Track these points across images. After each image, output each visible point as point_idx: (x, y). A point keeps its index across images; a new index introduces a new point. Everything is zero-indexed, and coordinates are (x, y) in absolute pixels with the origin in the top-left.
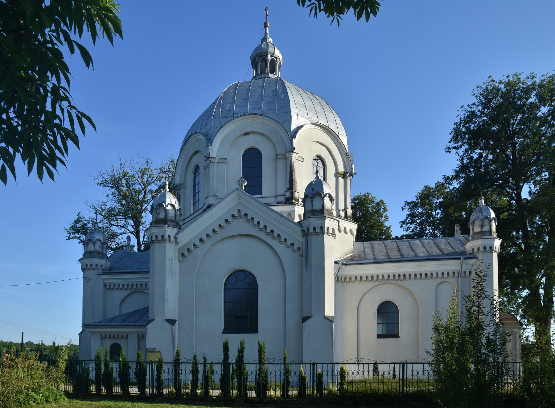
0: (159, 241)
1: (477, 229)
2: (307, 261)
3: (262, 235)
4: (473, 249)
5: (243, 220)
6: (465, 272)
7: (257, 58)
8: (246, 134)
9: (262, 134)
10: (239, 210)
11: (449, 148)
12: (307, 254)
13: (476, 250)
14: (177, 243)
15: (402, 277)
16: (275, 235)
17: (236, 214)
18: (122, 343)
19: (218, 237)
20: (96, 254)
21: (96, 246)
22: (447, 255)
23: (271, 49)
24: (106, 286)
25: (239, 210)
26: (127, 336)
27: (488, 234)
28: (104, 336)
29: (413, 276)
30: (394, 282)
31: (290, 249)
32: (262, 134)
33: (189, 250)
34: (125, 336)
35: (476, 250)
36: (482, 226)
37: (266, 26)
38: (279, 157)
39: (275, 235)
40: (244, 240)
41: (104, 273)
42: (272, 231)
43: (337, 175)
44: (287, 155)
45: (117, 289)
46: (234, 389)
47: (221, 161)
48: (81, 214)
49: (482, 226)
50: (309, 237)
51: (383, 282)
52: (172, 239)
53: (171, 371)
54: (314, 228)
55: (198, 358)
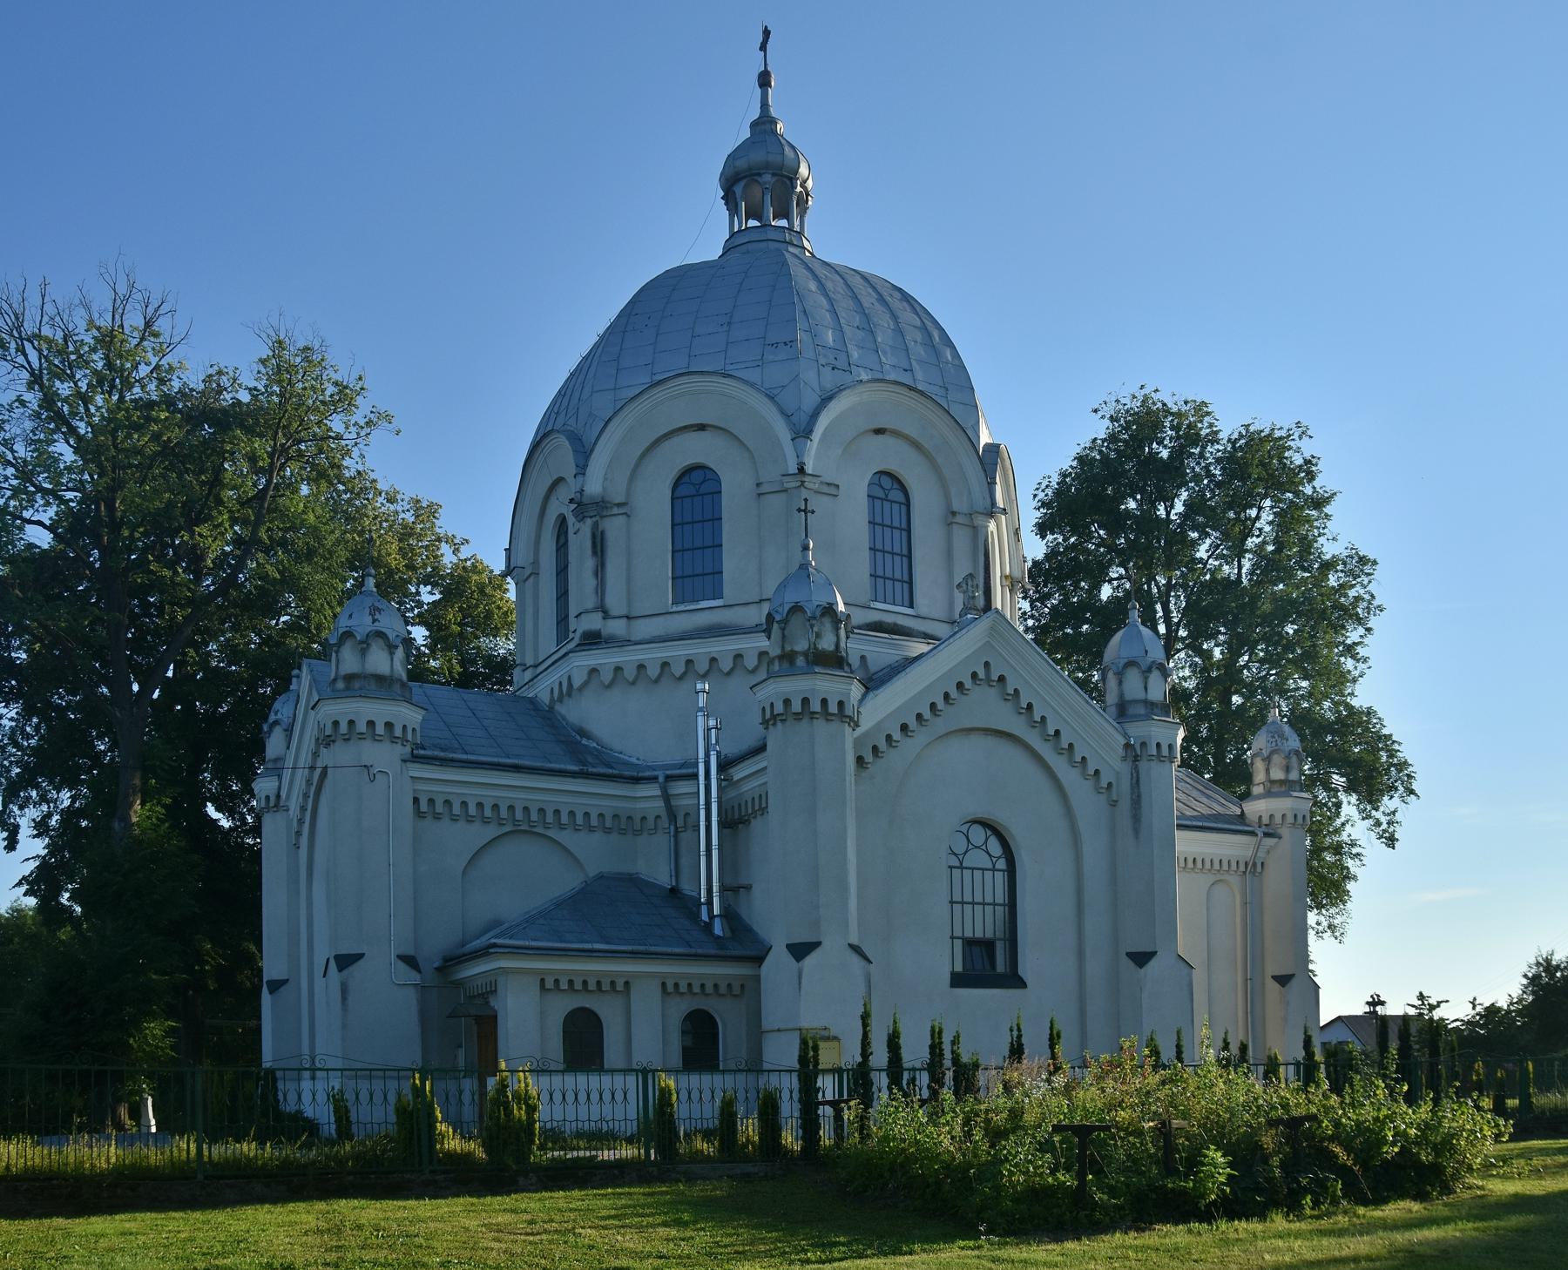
1: (1277, 774)
2: (1136, 818)
5: (993, 691)
9: (916, 445)
10: (987, 664)
12: (1136, 802)
13: (1278, 819)
17: (981, 675)
18: (608, 1011)
19: (940, 725)
23: (803, 170)
24: (416, 800)
25: (987, 664)
28: (549, 984)
31: (1089, 784)
32: (916, 445)
33: (875, 748)
34: (620, 987)
35: (1278, 819)
37: (764, 80)
38: (959, 519)
40: (990, 741)
41: (415, 758)
45: (454, 819)
47: (825, 489)
49: (1288, 769)
50: (1143, 765)
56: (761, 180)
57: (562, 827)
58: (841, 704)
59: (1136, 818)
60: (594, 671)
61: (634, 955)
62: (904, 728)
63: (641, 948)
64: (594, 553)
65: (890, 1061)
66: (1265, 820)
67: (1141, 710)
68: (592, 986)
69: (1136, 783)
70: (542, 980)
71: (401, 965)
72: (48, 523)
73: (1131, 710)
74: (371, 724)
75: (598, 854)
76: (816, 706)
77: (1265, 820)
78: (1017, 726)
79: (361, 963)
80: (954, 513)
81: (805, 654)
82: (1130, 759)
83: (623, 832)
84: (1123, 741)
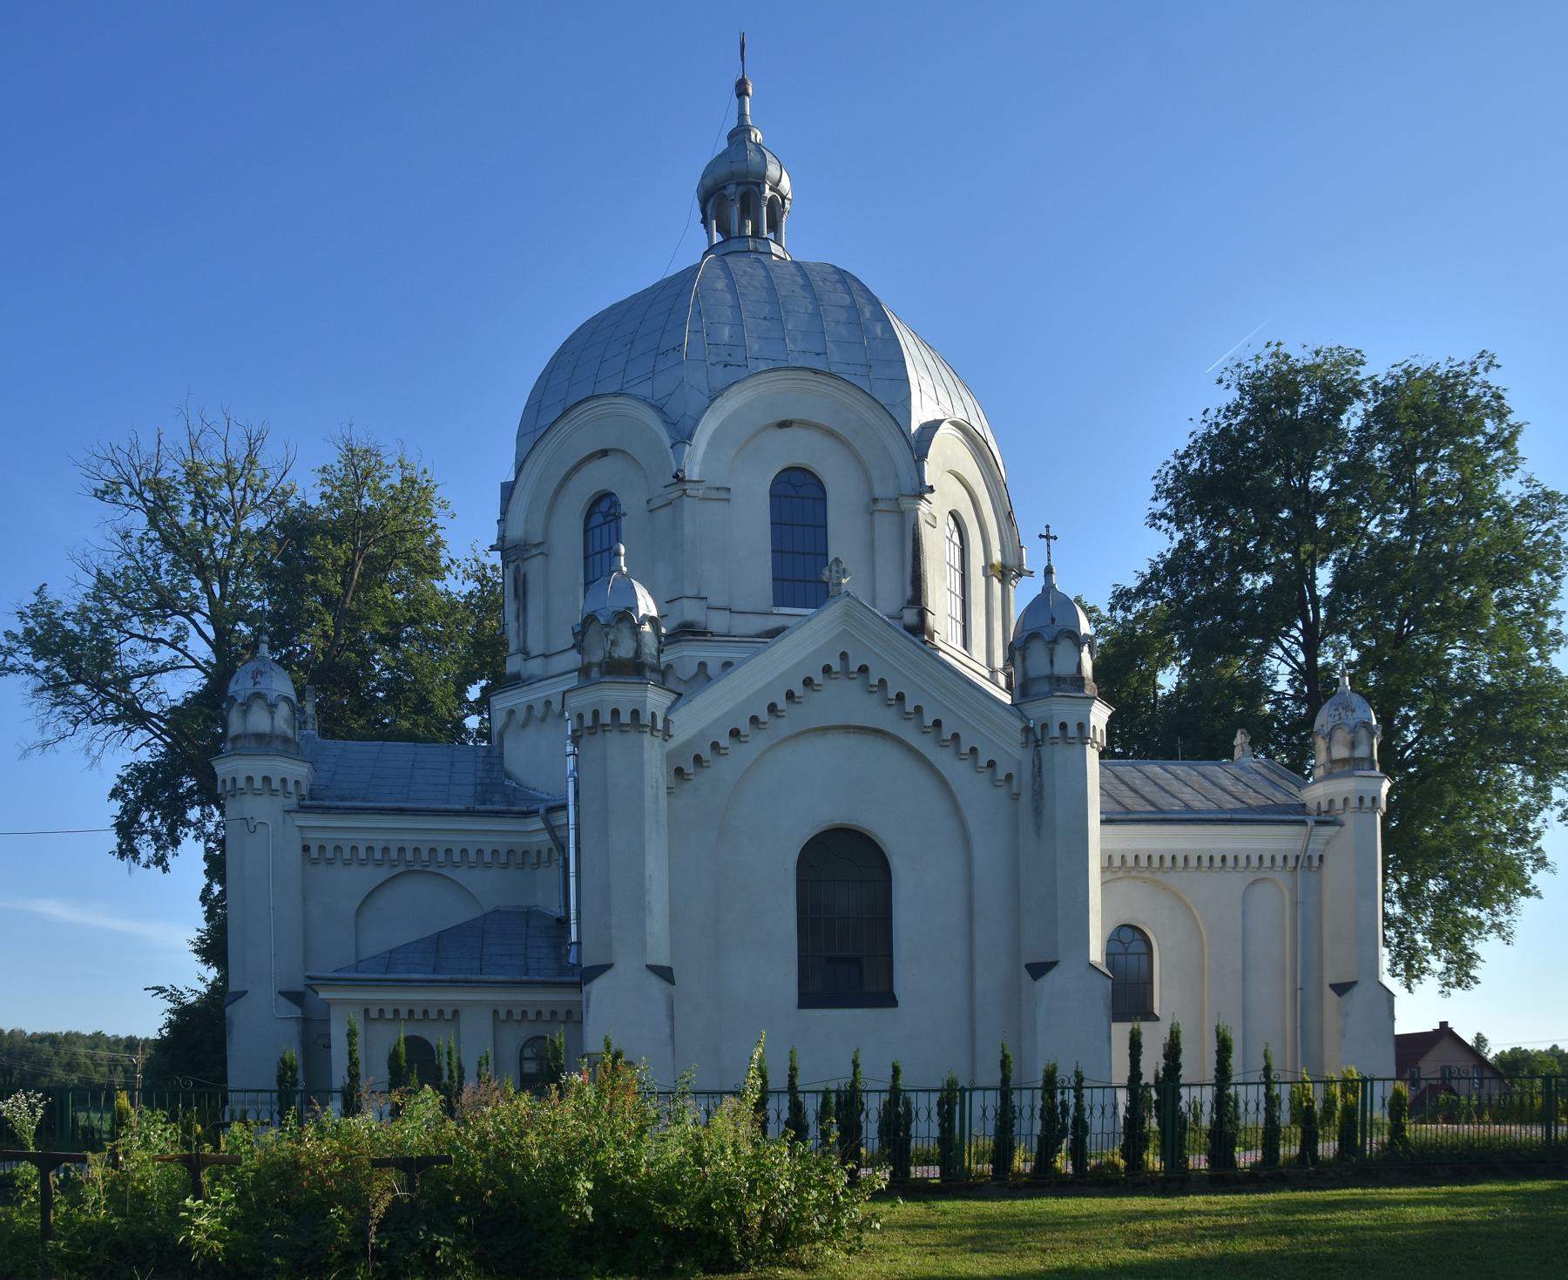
0: (622, 728)
1: (1340, 752)
2: (1038, 811)
3: (908, 733)
4: (1331, 802)
6: (1310, 858)
7: (732, 188)
8: (783, 425)
9: (830, 433)
10: (844, 656)
11: (1154, 516)
12: (1038, 793)
13: (1339, 804)
14: (667, 735)
15: (1168, 862)
16: (947, 734)
17: (836, 666)
19: (784, 727)
20: (278, 744)
21: (277, 716)
22: (1251, 809)
23: (773, 170)
24: (306, 849)
25: (844, 656)
26: (456, 1013)
27: (1367, 766)
28: (374, 1014)
29: (1193, 862)
30: (1146, 874)
32: (830, 433)
34: (448, 1015)
35: (1339, 804)
36: (1353, 745)
37: (741, 90)
38: (881, 506)
39: (947, 734)
40: (853, 741)
41: (303, 809)
42: (937, 723)
43: (988, 568)
44: (906, 504)
45: (347, 863)
46: (1248, 1147)
47: (714, 494)
48: (47, 590)
49: (1353, 745)
50: (1046, 751)
51: (1120, 874)
52: (660, 725)
53: (991, 1113)
54: (1063, 726)
55: (1059, 1075)
56: (734, 197)
57: (455, 865)
58: (635, 714)
59: (1038, 811)
60: (511, 712)
61: (453, 984)
62: (735, 733)
63: (462, 977)
64: (516, 596)
65: (1130, 1080)
66: (1324, 807)
67: (1045, 688)
68: (418, 1014)
69: (1038, 771)
70: (367, 1011)
71: (282, 1000)
72: (168, 639)
73: (1034, 689)
74: (250, 779)
75: (491, 890)
76: (606, 718)
77: (1324, 807)
78: (886, 719)
79: (244, 1000)
80: (875, 500)
81: (599, 665)
82: (1032, 744)
83: (521, 866)
84: (1020, 725)
